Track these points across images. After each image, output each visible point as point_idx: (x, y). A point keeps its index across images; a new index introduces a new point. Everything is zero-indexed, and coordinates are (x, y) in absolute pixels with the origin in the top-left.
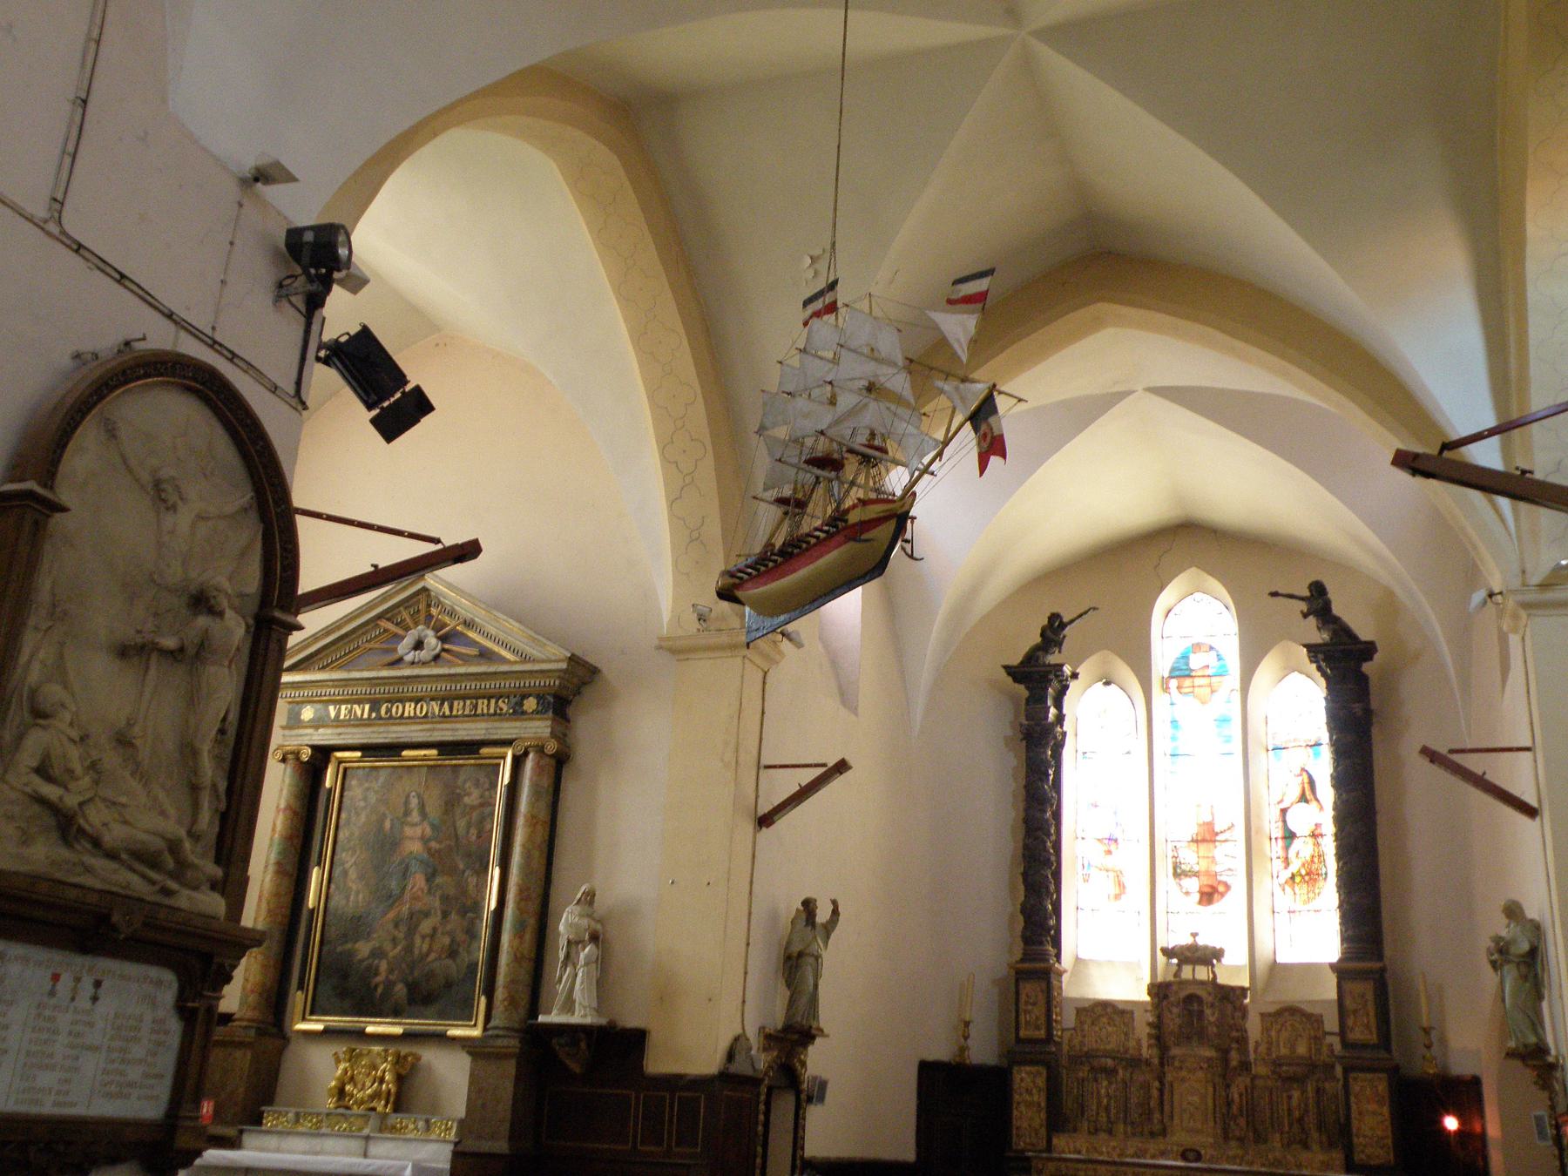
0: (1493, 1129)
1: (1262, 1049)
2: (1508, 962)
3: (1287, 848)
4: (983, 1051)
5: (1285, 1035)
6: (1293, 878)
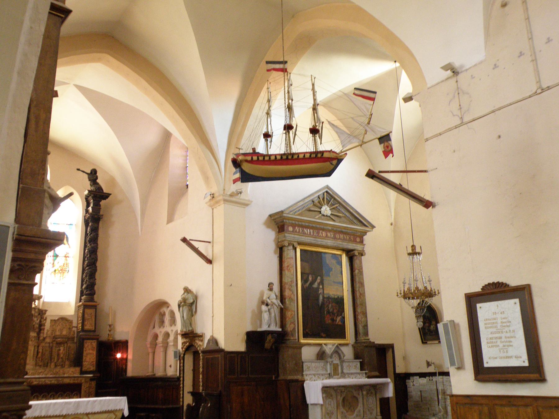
0: (130, 357)
1: (49, 333)
2: (185, 305)
3: (54, 260)
4: (269, 323)
5: (59, 328)
6: (55, 271)
